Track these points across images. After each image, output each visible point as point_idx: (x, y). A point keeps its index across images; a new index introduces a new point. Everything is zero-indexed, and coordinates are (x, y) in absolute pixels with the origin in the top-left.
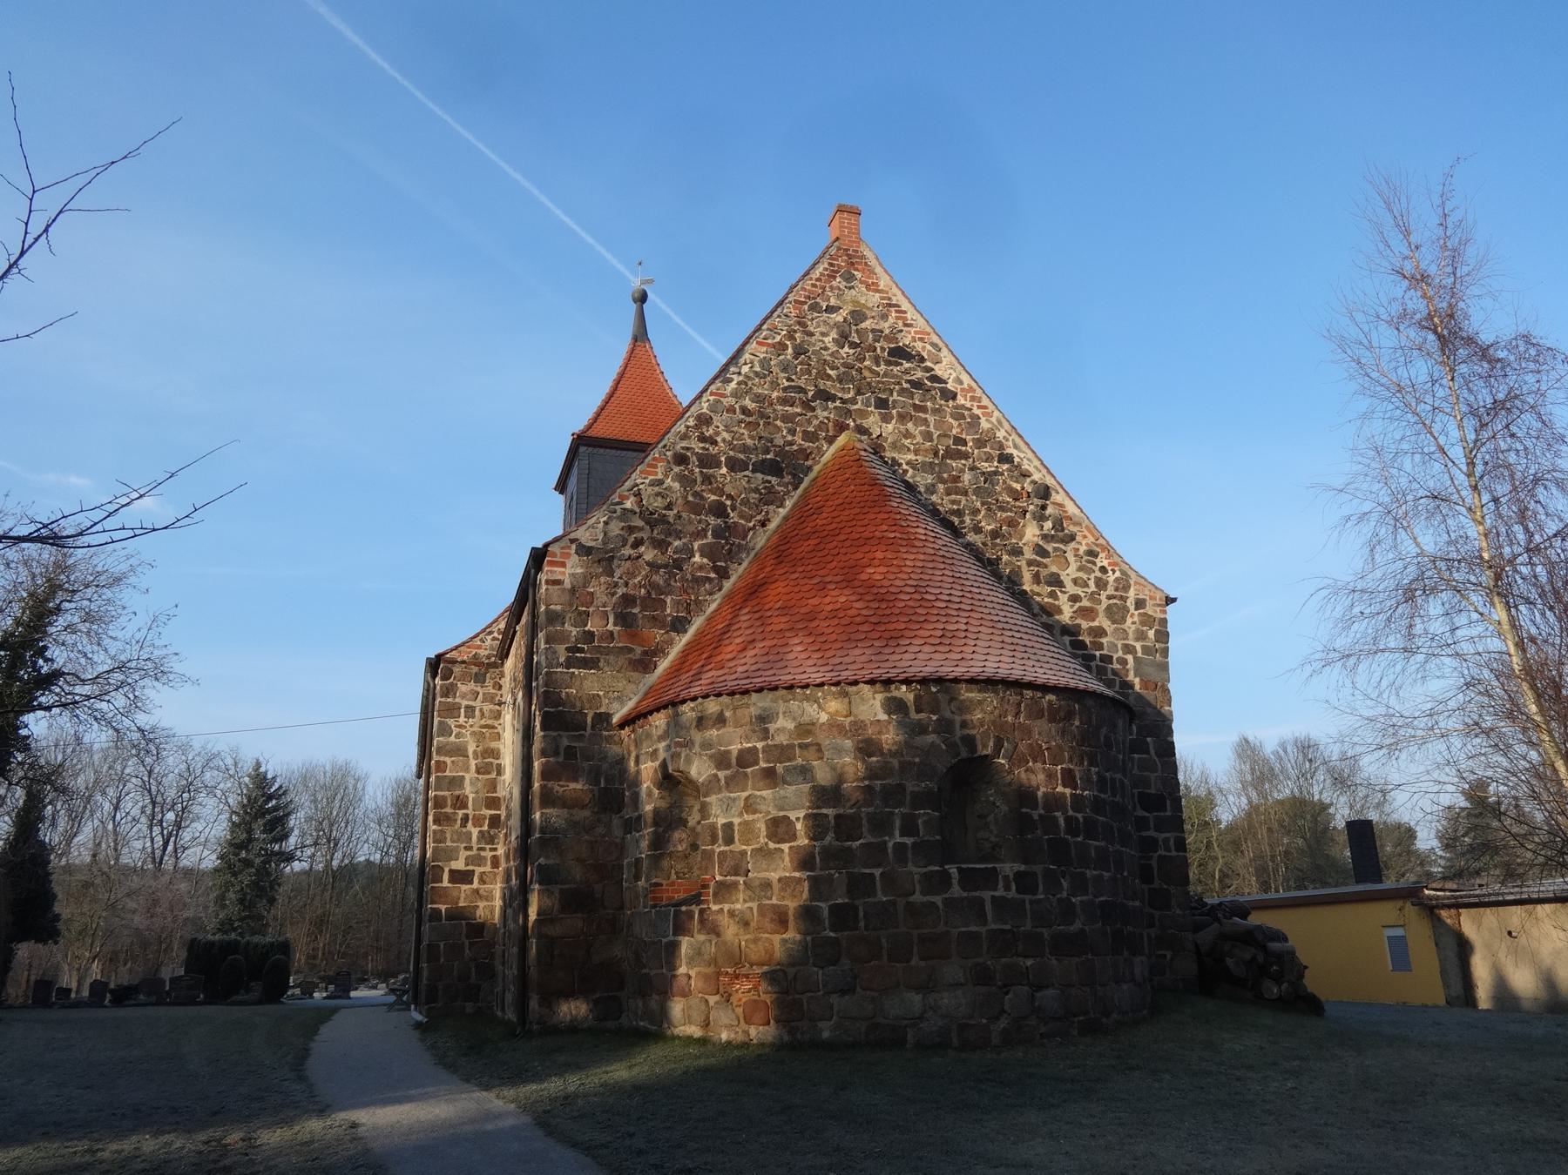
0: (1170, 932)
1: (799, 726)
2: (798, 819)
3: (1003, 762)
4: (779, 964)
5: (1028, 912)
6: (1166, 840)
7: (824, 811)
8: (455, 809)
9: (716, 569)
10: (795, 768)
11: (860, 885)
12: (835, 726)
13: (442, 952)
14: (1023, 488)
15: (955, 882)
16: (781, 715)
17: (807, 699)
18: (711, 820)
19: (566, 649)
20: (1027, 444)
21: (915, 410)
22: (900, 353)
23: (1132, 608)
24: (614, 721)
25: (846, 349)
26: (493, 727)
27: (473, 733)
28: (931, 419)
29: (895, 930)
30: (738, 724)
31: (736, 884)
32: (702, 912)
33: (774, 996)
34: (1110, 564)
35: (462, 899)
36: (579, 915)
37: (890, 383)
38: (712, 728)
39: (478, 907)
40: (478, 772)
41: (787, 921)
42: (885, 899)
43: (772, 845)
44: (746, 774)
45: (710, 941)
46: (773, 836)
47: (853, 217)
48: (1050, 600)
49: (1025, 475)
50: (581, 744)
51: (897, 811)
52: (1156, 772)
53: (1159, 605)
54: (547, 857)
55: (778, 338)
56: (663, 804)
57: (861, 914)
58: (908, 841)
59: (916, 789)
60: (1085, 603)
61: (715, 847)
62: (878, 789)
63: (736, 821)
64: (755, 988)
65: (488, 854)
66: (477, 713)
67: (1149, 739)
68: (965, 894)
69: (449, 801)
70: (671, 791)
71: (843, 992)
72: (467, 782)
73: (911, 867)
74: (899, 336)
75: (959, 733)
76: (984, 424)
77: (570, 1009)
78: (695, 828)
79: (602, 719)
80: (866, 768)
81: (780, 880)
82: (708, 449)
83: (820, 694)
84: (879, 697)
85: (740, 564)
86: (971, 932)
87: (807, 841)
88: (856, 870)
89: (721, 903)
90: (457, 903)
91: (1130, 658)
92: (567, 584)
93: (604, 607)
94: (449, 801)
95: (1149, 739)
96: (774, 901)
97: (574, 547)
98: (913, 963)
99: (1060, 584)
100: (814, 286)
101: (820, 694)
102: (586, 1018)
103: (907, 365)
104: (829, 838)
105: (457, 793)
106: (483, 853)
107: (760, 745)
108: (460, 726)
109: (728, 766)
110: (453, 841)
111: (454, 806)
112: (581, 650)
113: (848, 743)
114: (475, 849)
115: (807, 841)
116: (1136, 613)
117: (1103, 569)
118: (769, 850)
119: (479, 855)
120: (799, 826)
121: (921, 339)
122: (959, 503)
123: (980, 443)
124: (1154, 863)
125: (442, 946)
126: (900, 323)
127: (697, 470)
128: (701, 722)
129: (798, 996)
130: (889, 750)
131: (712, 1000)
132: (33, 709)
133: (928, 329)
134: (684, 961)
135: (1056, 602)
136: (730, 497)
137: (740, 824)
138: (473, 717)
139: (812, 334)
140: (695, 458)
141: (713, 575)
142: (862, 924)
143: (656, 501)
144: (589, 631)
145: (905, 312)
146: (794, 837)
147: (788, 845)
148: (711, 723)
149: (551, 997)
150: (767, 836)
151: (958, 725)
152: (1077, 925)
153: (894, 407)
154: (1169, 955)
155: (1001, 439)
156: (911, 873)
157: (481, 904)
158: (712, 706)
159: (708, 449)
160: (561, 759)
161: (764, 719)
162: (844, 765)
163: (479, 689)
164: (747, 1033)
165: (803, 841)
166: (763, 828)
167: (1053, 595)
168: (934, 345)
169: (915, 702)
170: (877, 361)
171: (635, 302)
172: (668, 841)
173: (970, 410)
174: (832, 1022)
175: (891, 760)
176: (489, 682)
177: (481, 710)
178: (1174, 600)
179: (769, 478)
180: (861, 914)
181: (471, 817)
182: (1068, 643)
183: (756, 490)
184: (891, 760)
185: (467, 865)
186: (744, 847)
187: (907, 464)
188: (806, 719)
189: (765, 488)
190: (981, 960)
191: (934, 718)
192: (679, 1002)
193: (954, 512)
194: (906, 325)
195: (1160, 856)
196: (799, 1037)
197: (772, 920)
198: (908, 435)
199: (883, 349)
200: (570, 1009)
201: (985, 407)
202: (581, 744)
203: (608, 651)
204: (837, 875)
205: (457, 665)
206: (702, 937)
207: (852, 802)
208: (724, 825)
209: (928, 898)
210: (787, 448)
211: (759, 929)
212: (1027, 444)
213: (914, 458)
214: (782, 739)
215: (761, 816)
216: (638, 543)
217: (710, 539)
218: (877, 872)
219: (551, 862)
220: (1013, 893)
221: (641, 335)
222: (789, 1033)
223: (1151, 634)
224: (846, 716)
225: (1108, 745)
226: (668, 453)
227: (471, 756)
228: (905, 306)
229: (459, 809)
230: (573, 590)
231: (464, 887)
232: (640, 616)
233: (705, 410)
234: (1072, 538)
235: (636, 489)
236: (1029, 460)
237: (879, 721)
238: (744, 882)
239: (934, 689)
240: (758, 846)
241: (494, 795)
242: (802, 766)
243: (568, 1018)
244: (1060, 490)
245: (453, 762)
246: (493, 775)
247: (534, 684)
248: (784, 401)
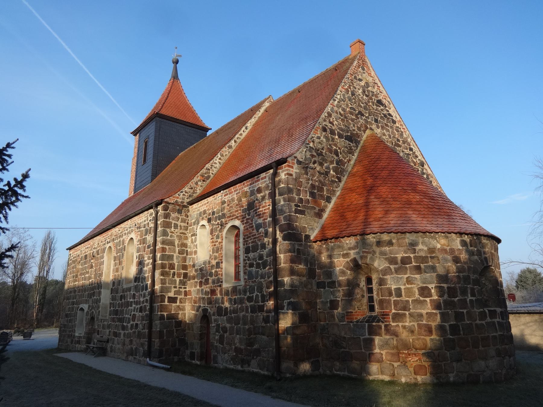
1: (429, 249)
2: (432, 288)
3: (493, 268)
4: (430, 349)
7: (442, 285)
8: (170, 269)
9: (338, 178)
10: (429, 266)
11: (459, 316)
12: (443, 250)
13: (165, 334)
16: (420, 244)
17: (432, 238)
18: (388, 286)
20: (416, 145)
21: (386, 126)
22: (380, 102)
26: (185, 234)
27: (177, 236)
30: (400, 245)
31: (405, 314)
32: (386, 326)
33: (429, 363)
35: (173, 310)
36: (305, 324)
37: (378, 113)
38: (385, 246)
39: (179, 313)
40: (179, 253)
41: (432, 331)
42: (468, 322)
43: (421, 299)
44: (406, 268)
45: (393, 339)
46: (421, 294)
47: (363, 45)
49: (417, 157)
50: (302, 248)
51: (468, 286)
54: (294, 299)
56: (351, 277)
57: (461, 329)
58: (474, 298)
59: (473, 278)
61: (391, 298)
62: (462, 277)
63: (403, 287)
64: (420, 359)
65: (183, 290)
70: (355, 271)
72: (175, 257)
73: (475, 310)
74: (379, 95)
75: (483, 256)
76: (405, 136)
77: (303, 367)
78: (362, 288)
79: (307, 237)
80: (456, 268)
81: (427, 313)
83: (437, 236)
84: (459, 239)
87: (437, 298)
88: (457, 310)
89: (397, 322)
90: (171, 312)
92: (294, 176)
93: (306, 188)
96: (424, 322)
97: (296, 160)
98: (480, 349)
101: (437, 236)
102: (308, 370)
104: (446, 296)
105: (171, 262)
106: (181, 290)
107: (412, 256)
109: (396, 263)
110: (169, 284)
111: (169, 268)
112: (299, 206)
113: (449, 257)
114: (178, 287)
115: (437, 298)
118: (420, 300)
119: (179, 290)
120: (433, 291)
123: (404, 142)
125: (165, 332)
126: (378, 91)
127: (330, 135)
128: (379, 243)
129: (440, 363)
130: (464, 261)
131: (396, 364)
132: (331, 265)
133: (387, 95)
134: (377, 347)
137: (405, 289)
138: (177, 229)
142: (462, 333)
143: (319, 145)
144: (301, 198)
146: (431, 296)
147: (429, 299)
148: (385, 244)
149: (298, 361)
150: (419, 295)
153: (380, 123)
156: (475, 311)
157: (180, 312)
158: (385, 237)
160: (296, 254)
161: (413, 245)
162: (448, 266)
163: (179, 216)
164: (416, 379)
165: (435, 297)
166: (417, 291)
168: (388, 102)
169: (470, 243)
170: (373, 103)
171: (173, 63)
172: (354, 294)
174: (454, 374)
175: (464, 265)
176: (183, 214)
180: (461, 329)
181: (176, 273)
183: (346, 147)
185: (175, 295)
186: (408, 299)
188: (431, 246)
189: (349, 147)
190: (497, 347)
192: (375, 365)
196: (441, 380)
197: (425, 331)
200: (303, 367)
203: (308, 208)
204: (450, 312)
205: (171, 204)
206: (388, 337)
207: (453, 282)
208: (395, 289)
211: (419, 334)
212: (416, 145)
214: (423, 254)
215: (415, 286)
216: (315, 163)
217: (335, 165)
218: (465, 311)
219: (295, 300)
221: (175, 77)
222: (437, 379)
224: (448, 246)
226: (321, 126)
227: (176, 246)
228: (379, 85)
229: (172, 269)
230: (296, 179)
231: (174, 305)
232: (317, 194)
233: (329, 111)
235: (313, 139)
238: (409, 314)
239: (475, 238)
240: (415, 298)
241: (185, 264)
242: (432, 266)
243: (303, 371)
244: (426, 164)
245: (169, 248)
246: (185, 255)
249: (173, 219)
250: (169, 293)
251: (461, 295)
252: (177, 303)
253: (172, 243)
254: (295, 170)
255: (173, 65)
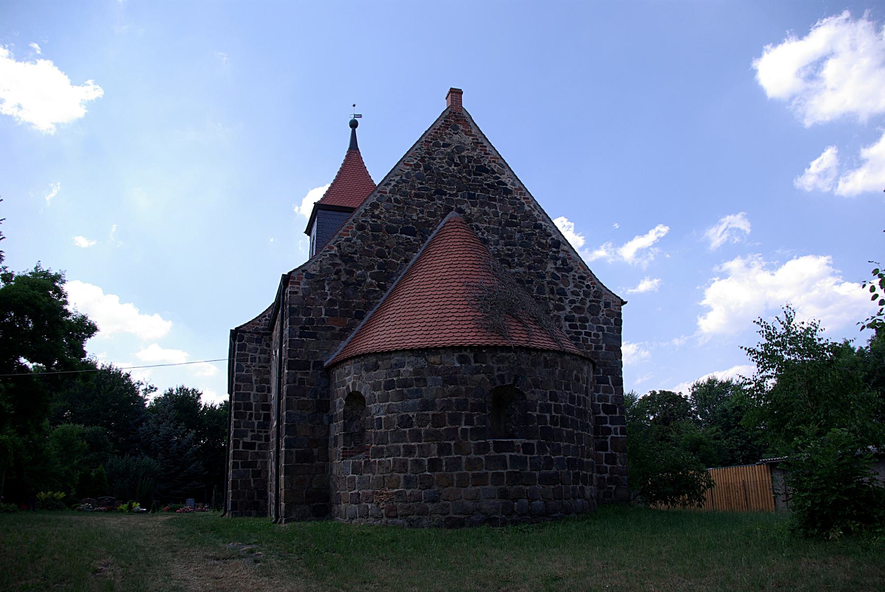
0: (615, 475)
5: (528, 463)
6: (616, 429)
14: (547, 242)
15: (492, 448)
19: (300, 327)
22: (482, 169)
23: (602, 308)
24: (325, 365)
25: (453, 167)
27: (255, 370)
28: (498, 205)
29: (461, 472)
34: (592, 284)
35: (249, 457)
40: (257, 391)
48: (559, 303)
49: (549, 235)
51: (463, 412)
52: (612, 393)
53: (617, 306)
55: (415, 161)
58: (469, 427)
59: (473, 402)
60: (578, 304)
65: (264, 434)
66: (257, 360)
67: (609, 376)
68: (496, 454)
69: (242, 407)
71: (433, 502)
72: (252, 396)
82: (376, 222)
85: (393, 283)
86: (498, 473)
91: (600, 333)
94: (242, 407)
95: (609, 376)
99: (565, 294)
100: (436, 133)
103: (486, 175)
106: (260, 434)
108: (248, 366)
110: (244, 427)
111: (245, 409)
116: (605, 309)
117: (588, 286)
121: (494, 162)
122: (511, 250)
124: (609, 441)
125: (239, 482)
127: (370, 233)
135: (562, 304)
136: (387, 247)
138: (255, 362)
139: (435, 159)
140: (369, 227)
141: (377, 289)
142: (444, 468)
145: (486, 147)
151: (496, 370)
152: (554, 469)
154: (614, 487)
155: (536, 216)
159: (376, 222)
160: (297, 384)
167: (561, 300)
173: (519, 200)
177: (259, 358)
178: (626, 303)
179: (409, 237)
182: (568, 326)
184: (461, 387)
185: (252, 439)
187: (484, 229)
190: (503, 486)
191: (484, 365)
193: (509, 255)
194: (485, 154)
195: (612, 437)
198: (485, 213)
199: (472, 166)
201: (528, 199)
202: (308, 377)
209: (478, 456)
210: (419, 221)
213: (488, 225)
217: (376, 270)
218: (452, 443)
220: (521, 454)
223: (612, 321)
224: (439, 365)
225: (577, 379)
231: (250, 451)
234: (571, 269)
236: (550, 227)
237: (456, 367)
247: (284, 346)
248: (416, 195)
249: (249, 351)
250: (244, 438)
251: (449, 423)
252: (255, 449)
253: (248, 380)
254: (302, 286)
255: (351, 129)
